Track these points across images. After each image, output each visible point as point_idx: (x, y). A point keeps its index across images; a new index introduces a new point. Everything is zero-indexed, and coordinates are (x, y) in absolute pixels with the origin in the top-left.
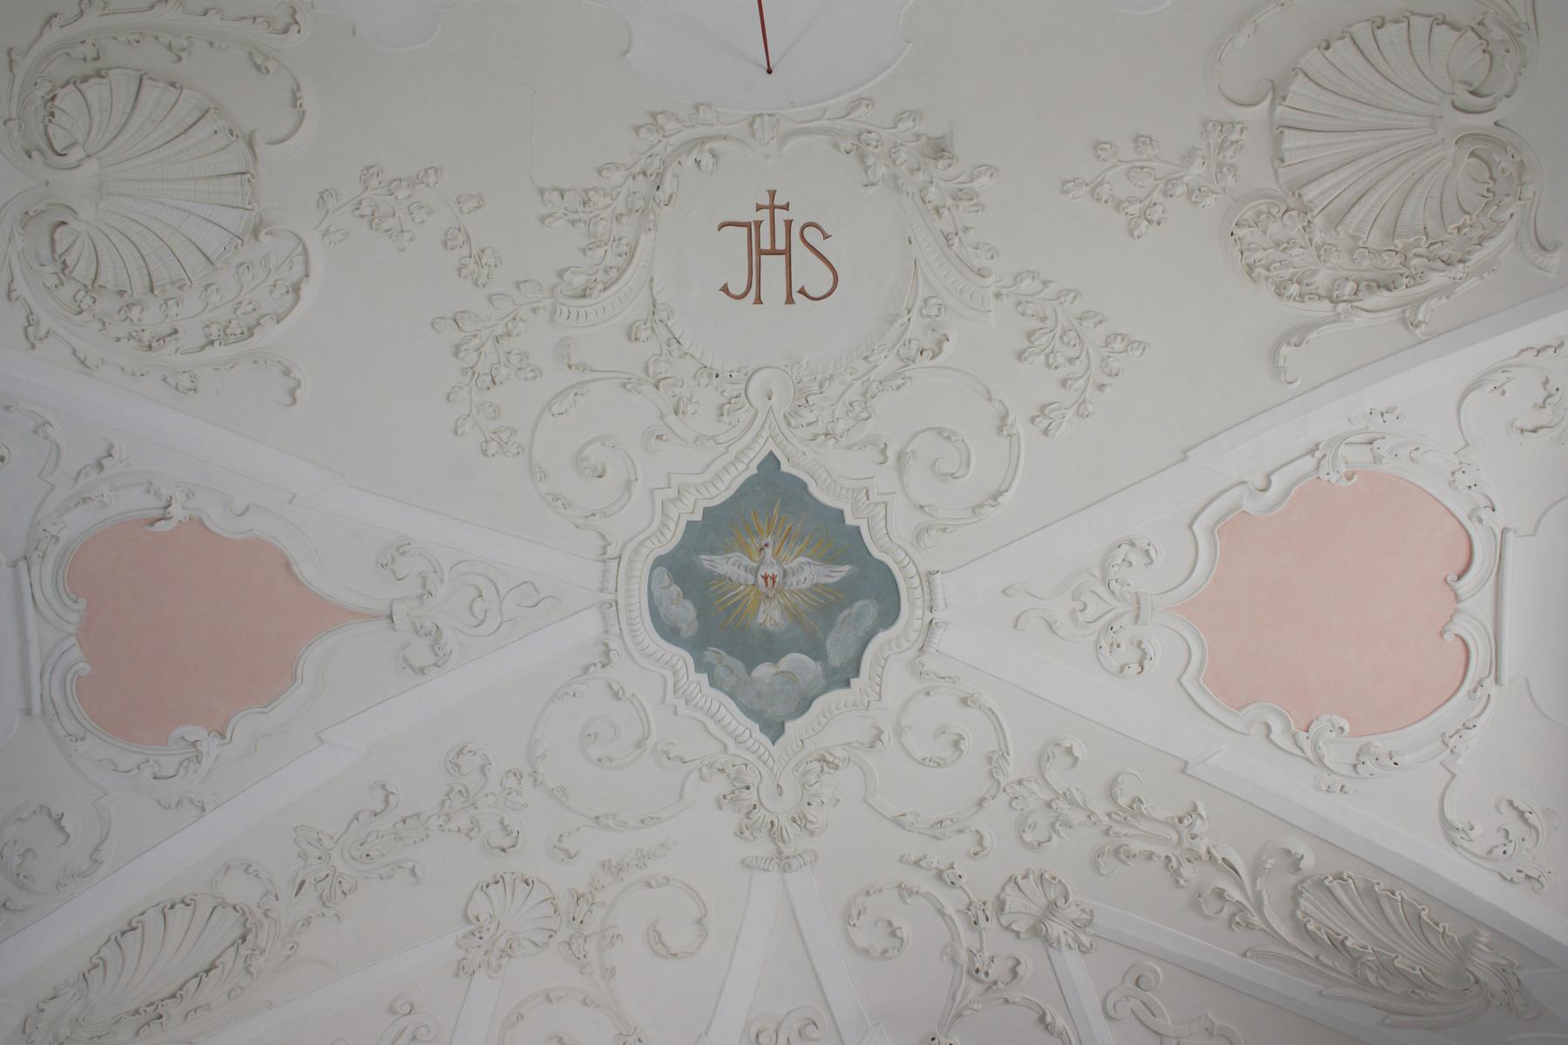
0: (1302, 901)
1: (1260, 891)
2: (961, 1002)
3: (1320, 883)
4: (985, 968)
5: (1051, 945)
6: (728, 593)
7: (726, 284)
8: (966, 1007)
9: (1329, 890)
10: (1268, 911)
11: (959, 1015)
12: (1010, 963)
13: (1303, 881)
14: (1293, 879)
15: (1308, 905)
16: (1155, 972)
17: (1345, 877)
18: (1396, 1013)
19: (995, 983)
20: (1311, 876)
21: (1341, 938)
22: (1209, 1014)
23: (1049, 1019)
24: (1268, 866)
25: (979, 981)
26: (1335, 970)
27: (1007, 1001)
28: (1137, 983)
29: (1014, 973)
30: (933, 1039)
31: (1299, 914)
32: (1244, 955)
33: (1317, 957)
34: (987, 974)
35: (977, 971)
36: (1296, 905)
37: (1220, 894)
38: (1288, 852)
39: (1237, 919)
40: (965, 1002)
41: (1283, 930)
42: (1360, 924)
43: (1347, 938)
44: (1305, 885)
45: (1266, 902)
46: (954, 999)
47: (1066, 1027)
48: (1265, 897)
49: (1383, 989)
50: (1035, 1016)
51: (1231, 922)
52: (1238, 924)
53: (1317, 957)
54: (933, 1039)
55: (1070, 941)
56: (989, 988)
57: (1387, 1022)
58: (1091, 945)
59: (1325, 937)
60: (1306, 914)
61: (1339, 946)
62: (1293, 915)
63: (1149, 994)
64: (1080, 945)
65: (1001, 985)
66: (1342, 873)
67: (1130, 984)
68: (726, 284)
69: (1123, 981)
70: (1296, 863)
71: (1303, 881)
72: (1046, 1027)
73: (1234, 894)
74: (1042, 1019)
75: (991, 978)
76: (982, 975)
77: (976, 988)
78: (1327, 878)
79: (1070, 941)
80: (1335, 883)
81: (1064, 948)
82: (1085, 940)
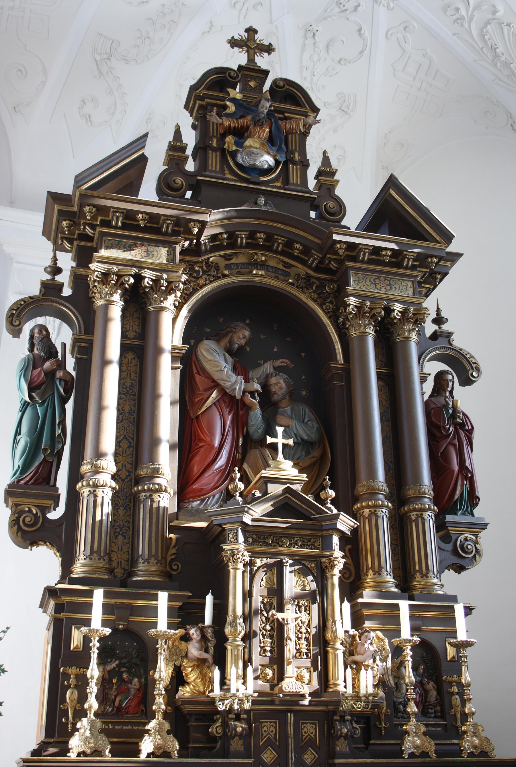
0: (489, 27)
1: (474, 16)
2: (328, 13)
3: (500, 24)
4: (344, 4)
5: (377, 3)
6: (219, 212)
7: (461, 255)
8: (330, 16)
9: (502, 28)
10: (473, 24)
11: (325, 19)
12: (356, 4)
13: (494, 19)
14: (490, 16)
15: (490, 29)
16: (414, 27)
17: (511, 26)
18: (500, 80)
19: (346, 10)
20: (499, 19)
21: (496, 47)
22: (428, 50)
23: (362, 32)
24: (483, 8)
25: (340, 8)
26: (487, 56)
27: (348, 19)
28: (405, 29)
29: (356, 8)
30: (311, 26)
31: (485, 30)
32: (454, 35)
33: (482, 48)
34: (344, 6)
35: (340, 4)
36: (485, 26)
37: (457, 9)
38: (494, 6)
39: (459, 21)
40: (330, 14)
41: (475, 33)
42: (506, 44)
43: (498, 48)
44: (494, 21)
45: (474, 21)
46: (326, 11)
47: (368, 38)
48: (475, 19)
49: (501, 70)
50: (357, 28)
51: (455, 21)
52: (458, 23)
53: (482, 48)
54: (311, 26)
55: (385, 4)
56: (342, 11)
57: (495, 82)
58: (393, 8)
59: (490, 44)
60: (487, 32)
61: (493, 49)
62: (482, 29)
63: (408, 34)
64: (388, 6)
65: (348, 12)
66: (511, 24)
67: (401, 28)
68: (461, 255)
69: (399, 26)
70: (495, 12)
71: (494, 19)
72: (360, 34)
73: (463, 12)
74: (360, 30)
75: (345, 8)
76: (342, 6)
77: (337, 9)
78: (503, 23)
79: (385, 4)
80: (506, 27)
81: (381, 5)
82: (392, 5)
